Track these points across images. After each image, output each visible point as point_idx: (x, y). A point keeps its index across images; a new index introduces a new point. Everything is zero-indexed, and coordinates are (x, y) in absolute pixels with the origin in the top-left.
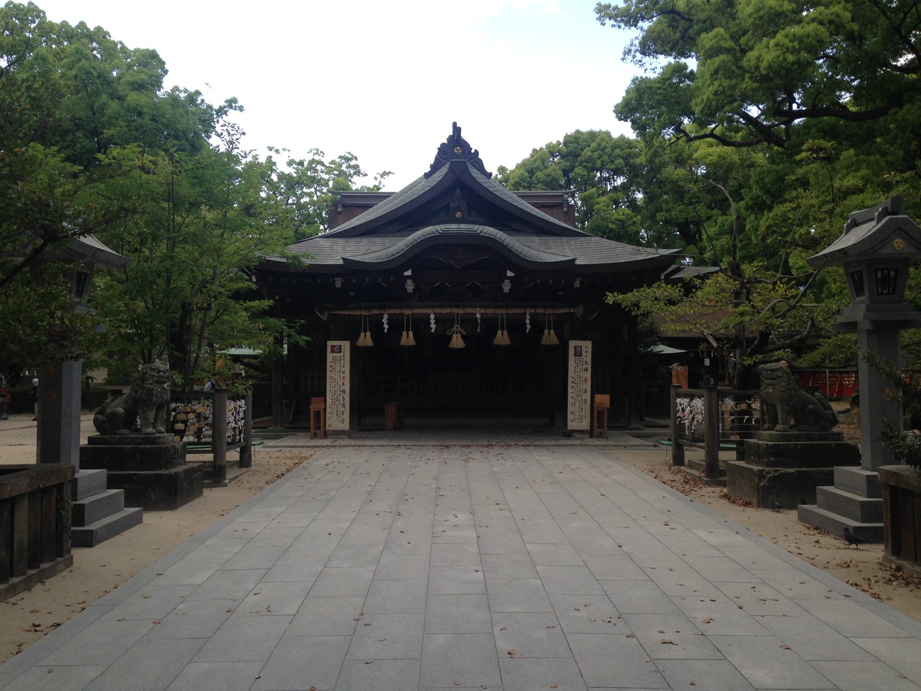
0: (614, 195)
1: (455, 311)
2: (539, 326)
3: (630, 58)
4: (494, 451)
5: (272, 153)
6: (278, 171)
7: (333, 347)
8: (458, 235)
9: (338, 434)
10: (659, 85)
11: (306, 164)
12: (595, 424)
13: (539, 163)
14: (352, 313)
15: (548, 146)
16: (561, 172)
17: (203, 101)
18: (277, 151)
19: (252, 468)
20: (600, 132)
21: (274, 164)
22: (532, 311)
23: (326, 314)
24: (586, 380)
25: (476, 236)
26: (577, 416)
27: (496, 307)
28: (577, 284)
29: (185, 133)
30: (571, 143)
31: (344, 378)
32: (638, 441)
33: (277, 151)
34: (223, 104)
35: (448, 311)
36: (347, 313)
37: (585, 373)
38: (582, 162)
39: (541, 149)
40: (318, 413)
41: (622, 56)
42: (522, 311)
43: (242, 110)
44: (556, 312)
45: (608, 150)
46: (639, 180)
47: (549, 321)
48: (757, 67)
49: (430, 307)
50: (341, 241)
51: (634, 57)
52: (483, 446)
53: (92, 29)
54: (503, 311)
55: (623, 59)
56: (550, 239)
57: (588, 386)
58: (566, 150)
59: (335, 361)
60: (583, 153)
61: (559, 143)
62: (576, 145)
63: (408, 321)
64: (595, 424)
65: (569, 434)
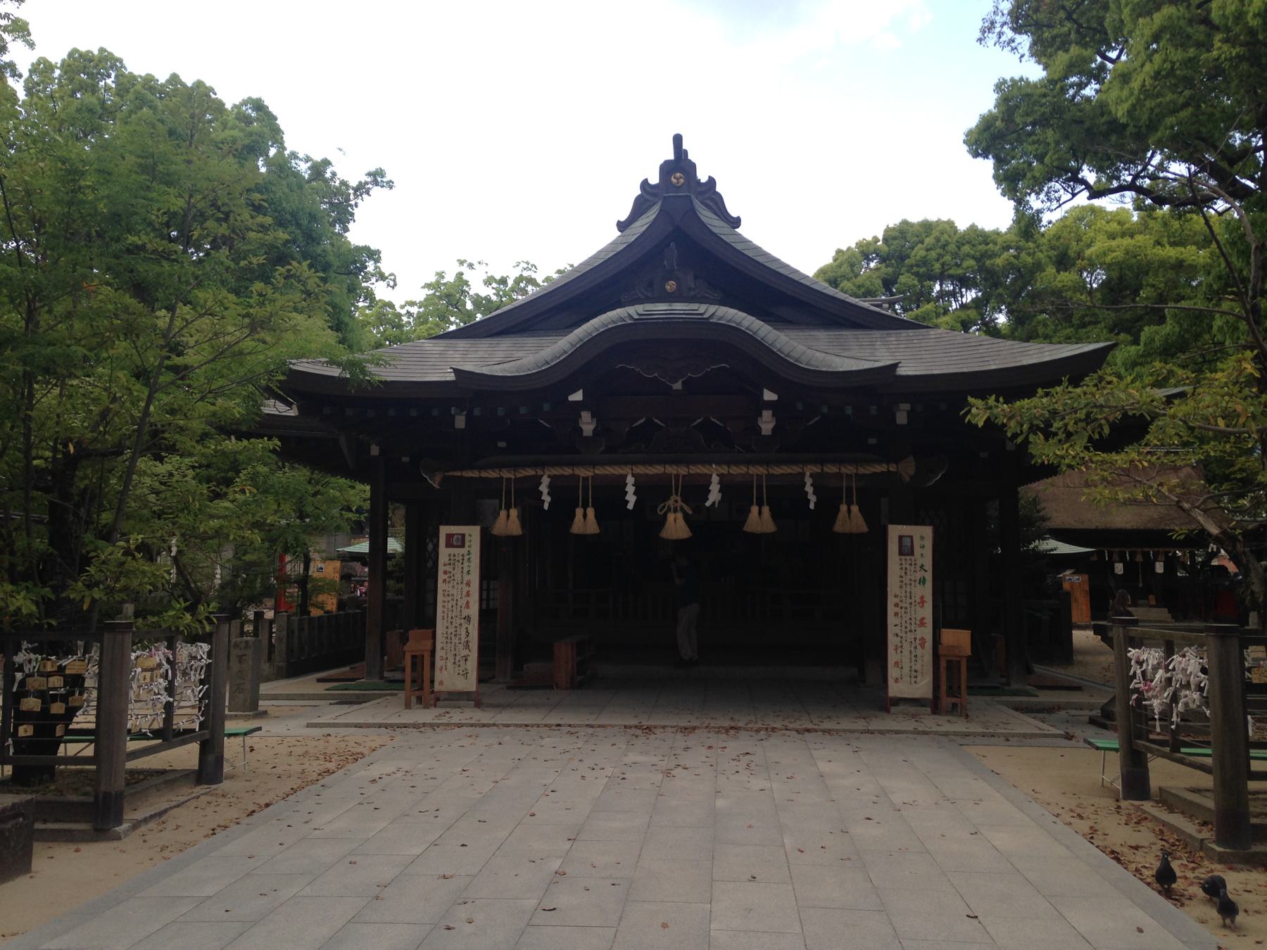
0: (963, 315)
1: (671, 470)
2: (830, 499)
3: (992, 38)
4: (735, 745)
5: (464, 269)
6: (471, 293)
7: (449, 536)
8: (668, 323)
9: (456, 698)
10: (1044, 90)
11: (510, 283)
12: (944, 688)
13: (845, 269)
14: (484, 474)
15: (859, 245)
16: (880, 282)
17: (334, 174)
18: (471, 266)
19: (225, 785)
20: (939, 222)
21: (466, 283)
22: (817, 469)
23: (438, 478)
24: (922, 602)
25: (704, 323)
26: (906, 670)
27: (748, 463)
28: (902, 418)
29: (293, 215)
30: (895, 238)
31: (468, 594)
32: (1027, 724)
33: (471, 266)
34: (365, 179)
35: (657, 470)
36: (458, 474)
37: (919, 587)
38: (912, 266)
39: (849, 248)
40: (417, 661)
41: (979, 35)
42: (795, 469)
43: (391, 188)
44: (862, 471)
45: (952, 247)
46: (1000, 290)
47: (849, 489)
48: (1239, 16)
49: (626, 463)
50: (462, 344)
51: (1000, 34)
52: (719, 730)
53: (189, 85)
54: (761, 470)
55: (980, 40)
56: (848, 334)
57: (927, 612)
58: (886, 249)
59: (452, 562)
60: (913, 253)
61: (876, 240)
62: (902, 242)
63: (585, 488)
64: (944, 688)
65: (886, 704)
